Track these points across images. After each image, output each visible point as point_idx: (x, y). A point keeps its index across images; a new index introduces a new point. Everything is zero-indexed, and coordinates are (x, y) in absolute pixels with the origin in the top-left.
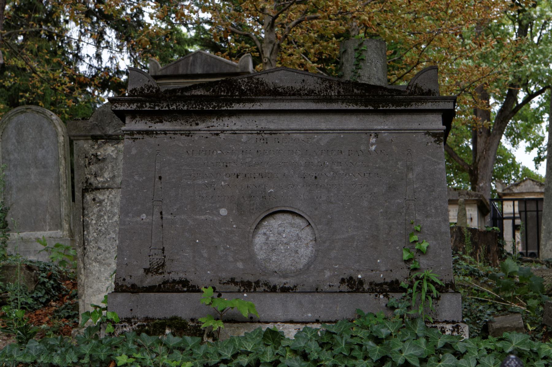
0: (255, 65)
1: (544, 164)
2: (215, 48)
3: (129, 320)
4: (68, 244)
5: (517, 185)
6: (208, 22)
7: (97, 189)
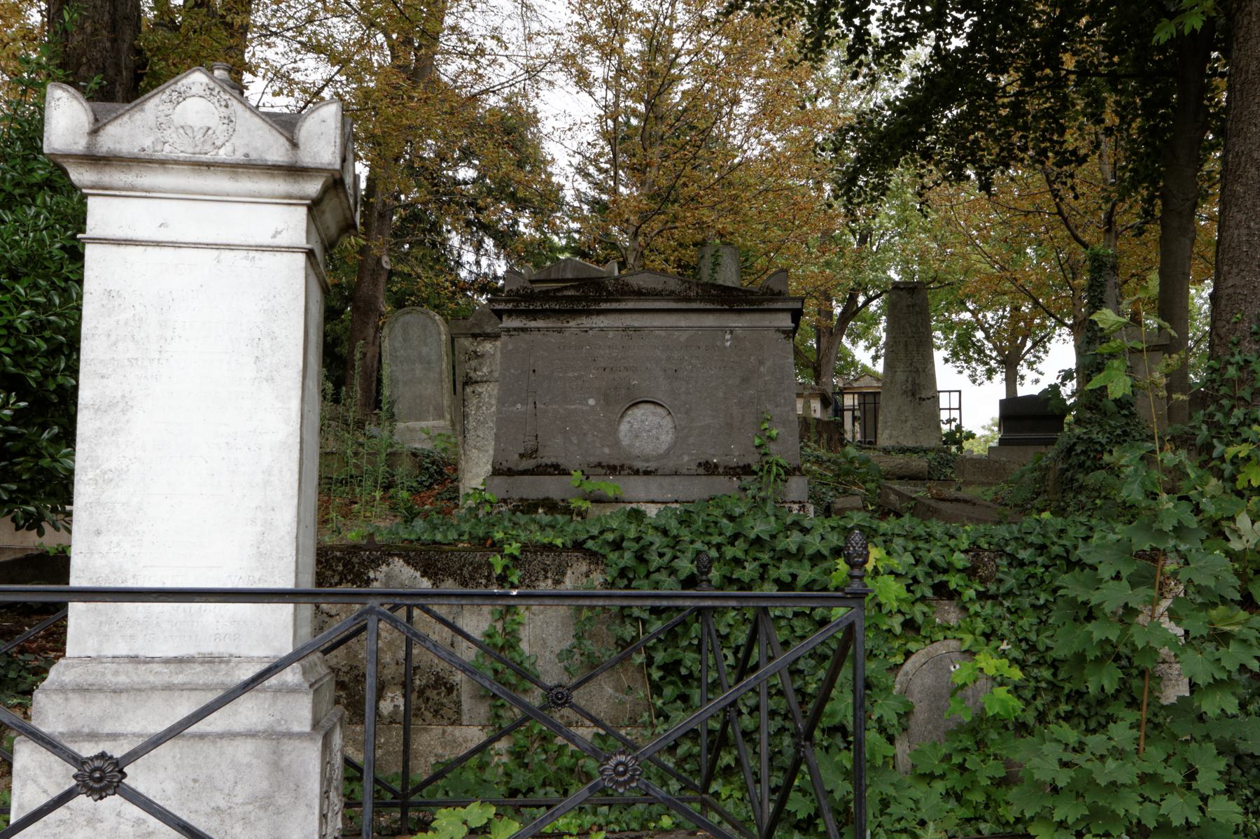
0: (620, 270)
1: (881, 361)
2: (584, 255)
3: (505, 501)
4: (450, 432)
5: (856, 380)
6: (578, 231)
7: (476, 382)
